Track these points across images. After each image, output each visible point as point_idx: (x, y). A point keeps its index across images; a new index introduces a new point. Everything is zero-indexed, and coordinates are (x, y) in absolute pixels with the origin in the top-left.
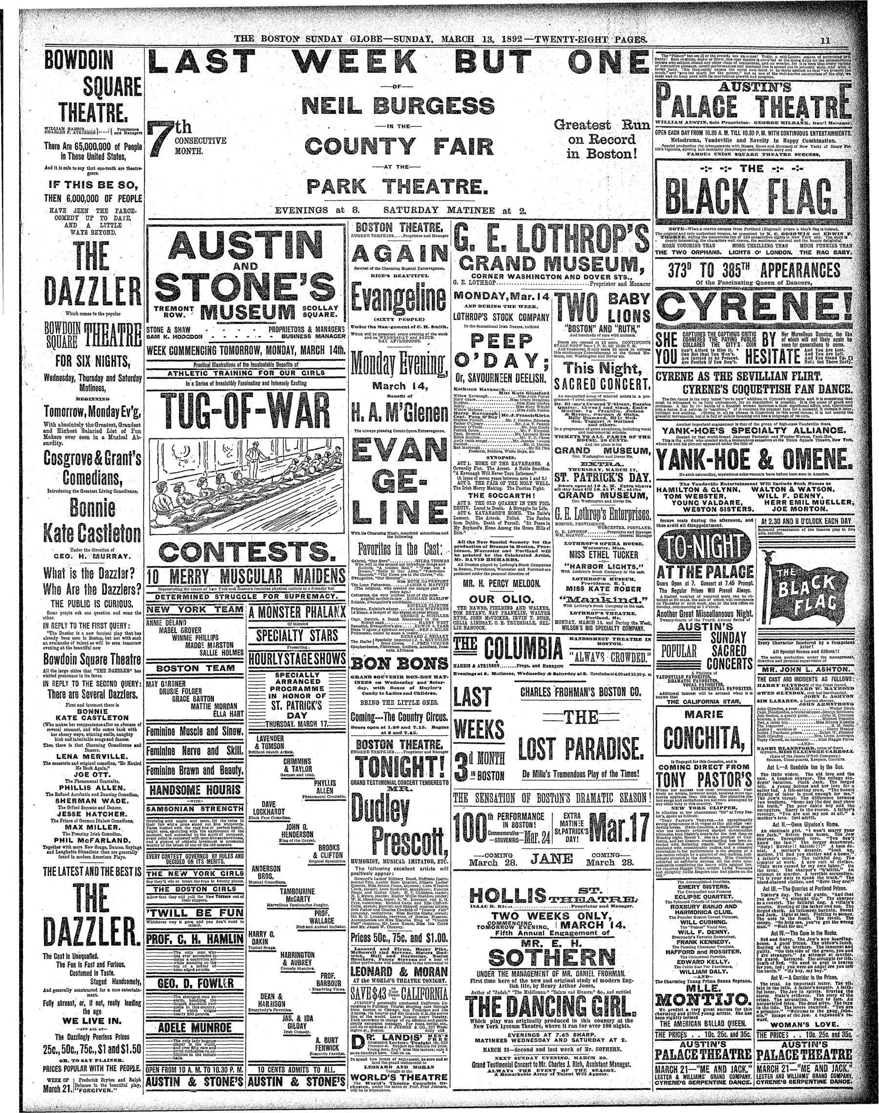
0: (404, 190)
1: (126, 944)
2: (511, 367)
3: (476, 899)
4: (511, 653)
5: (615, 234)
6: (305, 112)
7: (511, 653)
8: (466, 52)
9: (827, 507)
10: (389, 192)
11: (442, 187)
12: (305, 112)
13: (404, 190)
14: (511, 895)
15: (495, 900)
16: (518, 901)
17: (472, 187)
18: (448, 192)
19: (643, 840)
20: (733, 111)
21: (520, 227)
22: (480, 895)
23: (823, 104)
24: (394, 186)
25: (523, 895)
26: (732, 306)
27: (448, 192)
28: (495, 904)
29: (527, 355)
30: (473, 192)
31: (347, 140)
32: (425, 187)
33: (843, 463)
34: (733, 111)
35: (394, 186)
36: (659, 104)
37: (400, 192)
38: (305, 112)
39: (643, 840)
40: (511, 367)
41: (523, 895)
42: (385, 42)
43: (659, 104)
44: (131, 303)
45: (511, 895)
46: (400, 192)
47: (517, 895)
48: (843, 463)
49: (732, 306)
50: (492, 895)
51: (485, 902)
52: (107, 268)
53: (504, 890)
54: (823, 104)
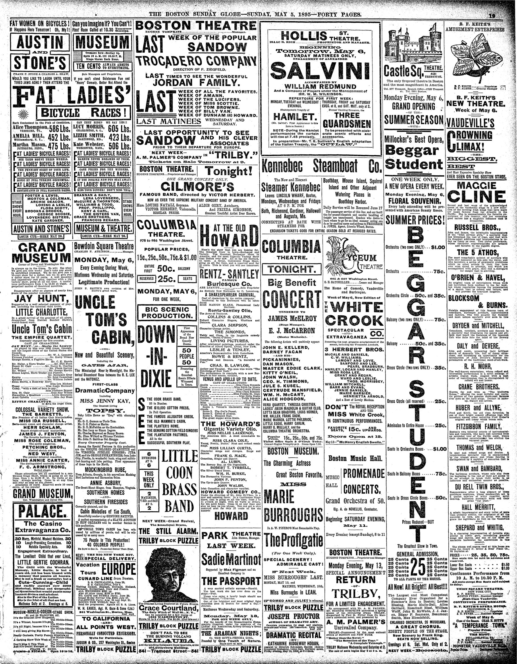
0: (209, 27)
1: (308, 307)
3: (285, 38)
9: (293, 362)
10: (200, 28)
11: (232, 26)
13: (209, 27)
14: (306, 35)
16: (311, 39)
17: (251, 26)
18: (236, 29)
19: (318, 307)
23: (206, 580)
25: (314, 36)
26: (416, 355)
27: (236, 29)
30: (251, 29)
32: (222, 26)
33: (60, 514)
37: (207, 28)
39: (318, 307)
41: (314, 36)
44: (308, 307)
45: (306, 35)
46: (207, 28)
47: (310, 36)
48: (60, 514)
49: (416, 355)
50: (295, 36)
51: (290, 39)
52: (114, 307)
53: (302, 33)
54: (206, 580)
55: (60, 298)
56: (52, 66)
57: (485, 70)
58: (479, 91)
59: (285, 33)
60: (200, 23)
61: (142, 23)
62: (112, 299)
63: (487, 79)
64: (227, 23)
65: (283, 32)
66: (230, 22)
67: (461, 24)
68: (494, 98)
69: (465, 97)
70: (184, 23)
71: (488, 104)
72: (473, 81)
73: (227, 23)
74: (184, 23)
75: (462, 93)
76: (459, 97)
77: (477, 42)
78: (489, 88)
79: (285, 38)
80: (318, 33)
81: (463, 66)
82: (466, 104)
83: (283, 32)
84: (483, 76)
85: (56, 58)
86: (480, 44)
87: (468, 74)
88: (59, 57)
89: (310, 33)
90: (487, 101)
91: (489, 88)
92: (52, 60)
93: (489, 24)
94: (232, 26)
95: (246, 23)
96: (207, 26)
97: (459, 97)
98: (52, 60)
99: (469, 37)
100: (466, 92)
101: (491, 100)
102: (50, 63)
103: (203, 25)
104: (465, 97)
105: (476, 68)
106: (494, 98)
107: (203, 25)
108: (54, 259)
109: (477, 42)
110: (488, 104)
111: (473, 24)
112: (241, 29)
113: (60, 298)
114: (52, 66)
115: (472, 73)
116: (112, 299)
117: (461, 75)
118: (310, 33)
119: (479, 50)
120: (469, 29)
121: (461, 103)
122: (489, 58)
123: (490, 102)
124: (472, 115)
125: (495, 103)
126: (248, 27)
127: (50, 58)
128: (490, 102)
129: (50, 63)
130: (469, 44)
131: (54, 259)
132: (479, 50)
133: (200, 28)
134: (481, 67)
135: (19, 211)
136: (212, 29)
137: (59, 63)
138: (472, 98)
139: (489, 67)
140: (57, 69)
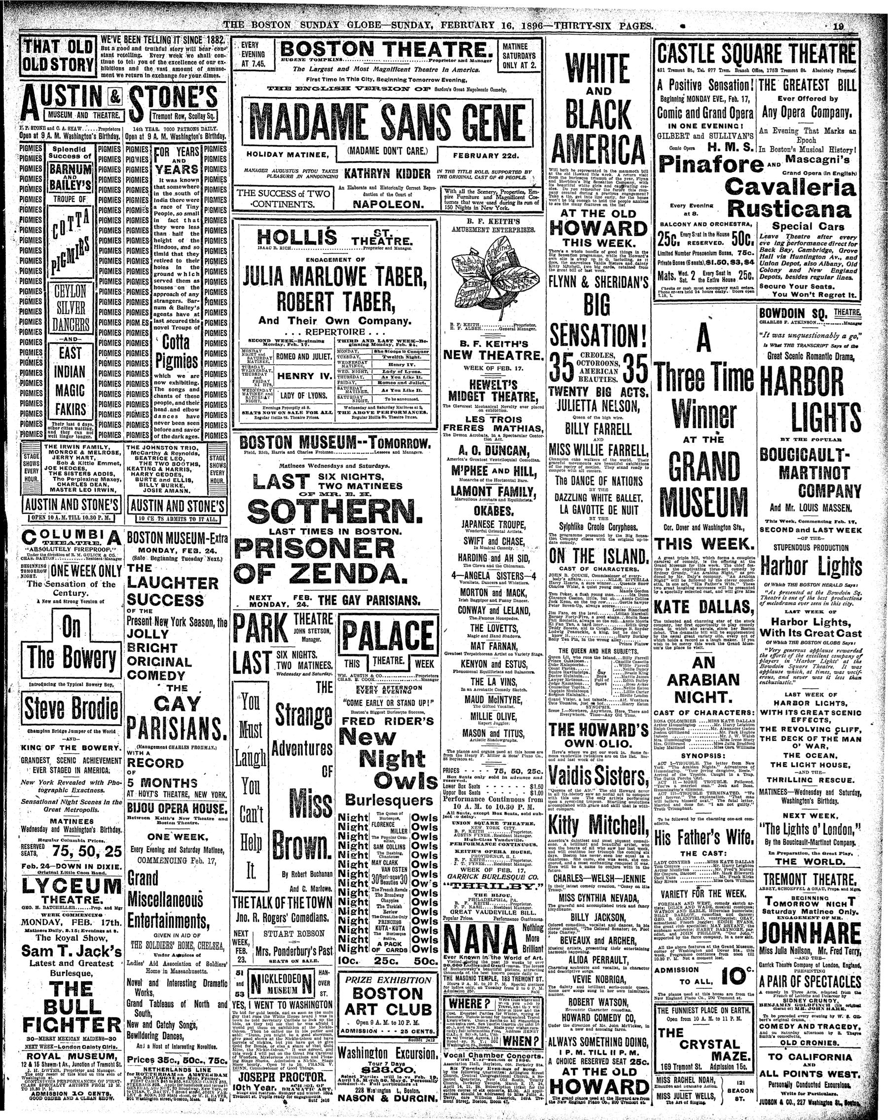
0: (405, 53)
2: (178, 710)
3: (264, 240)
4: (267, 279)
5: (345, 630)
6: (362, 765)
7: (267, 279)
8: (244, 540)
10: (389, 54)
11: (444, 50)
12: (362, 765)
13: (405, 53)
14: (300, 237)
15: (307, 53)
16: (308, 242)
17: (477, 49)
18: (450, 54)
20: (857, 938)
21: (117, 830)
22: (268, 236)
24: (664, 543)
26: (385, 549)
27: (450, 54)
28: (307, 58)
29: (190, 698)
31: (693, 170)
32: (427, 49)
34: (857, 938)
35: (664, 543)
36: (235, 632)
37: (401, 55)
38: (362, 765)
40: (178, 710)
41: (314, 237)
42: (545, 29)
43: (235, 632)
45: (300, 237)
46: (401, 55)
49: (385, 549)
55: (719, 697)
56: (194, 101)
57: (509, 298)
58: (503, 332)
59: (264, 233)
60: (389, 45)
61: (291, 44)
62: (856, 929)
63: (513, 314)
64: (435, 45)
65: (260, 232)
66: (440, 42)
67: (470, 221)
68: (525, 344)
69: (475, 343)
70: (363, 44)
71: (515, 355)
72: (487, 317)
73: (435, 45)
74: (363, 44)
75: (470, 336)
76: (463, 343)
77: (496, 251)
78: (521, 327)
79: (264, 240)
80: (320, 232)
81: (473, 292)
82: (476, 355)
83: (260, 232)
84: (506, 309)
85: (202, 88)
86: (502, 253)
87: (481, 304)
88: (206, 86)
89: (307, 232)
90: (514, 350)
91: (521, 327)
92: (195, 92)
93: (518, 221)
94: (444, 50)
95: (470, 45)
96: (401, 49)
97: (463, 343)
98: (195, 92)
99: (483, 242)
100: (470, 336)
101: (520, 348)
102: (192, 97)
103: (395, 49)
104: (475, 343)
105: (493, 294)
106: (525, 344)
107: (395, 49)
108: (93, 887)
109: (496, 251)
110: (515, 355)
111: (491, 222)
112: (461, 55)
113: (719, 697)
114: (194, 101)
115: (485, 303)
116: (856, 929)
117: (467, 306)
118: (307, 232)
119: (500, 265)
120: (483, 230)
121: (467, 355)
122: (516, 277)
123: (519, 352)
124: (486, 375)
125: (527, 355)
126: (472, 50)
127: (191, 88)
128: (519, 352)
129: (192, 97)
130: (482, 254)
131: (93, 887)
132: (500, 265)
133: (389, 54)
134: (503, 293)
135: (35, 471)
136: (409, 55)
137: (205, 97)
138: (488, 344)
139: (516, 294)
140: (203, 105)
